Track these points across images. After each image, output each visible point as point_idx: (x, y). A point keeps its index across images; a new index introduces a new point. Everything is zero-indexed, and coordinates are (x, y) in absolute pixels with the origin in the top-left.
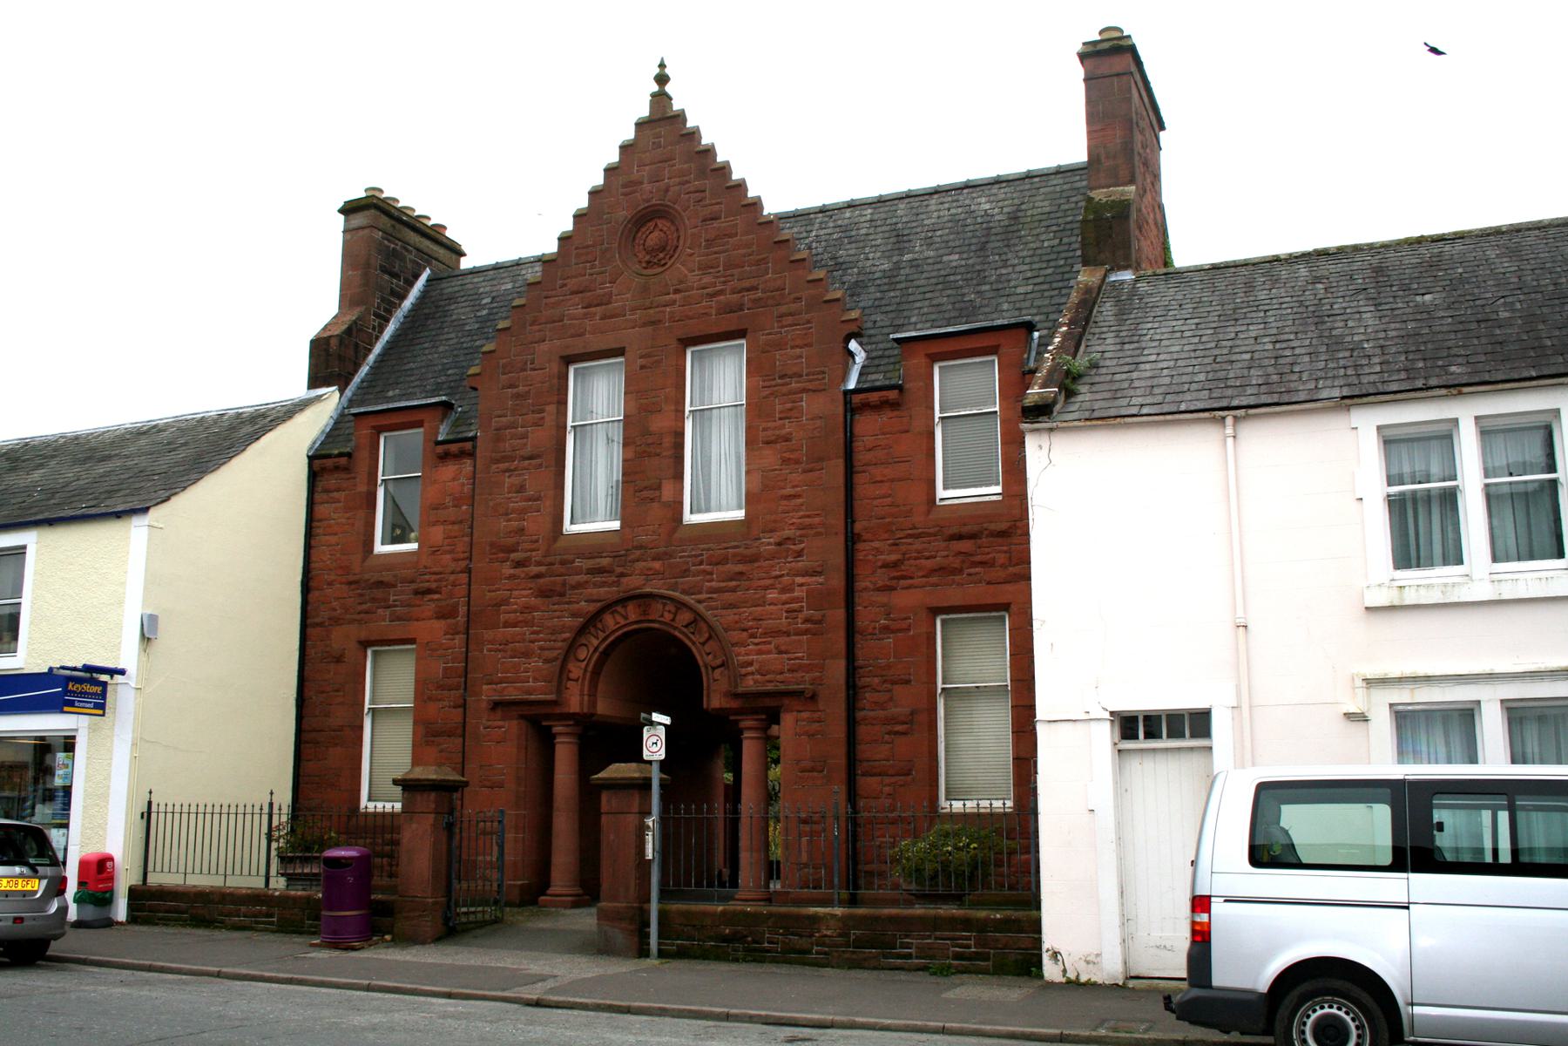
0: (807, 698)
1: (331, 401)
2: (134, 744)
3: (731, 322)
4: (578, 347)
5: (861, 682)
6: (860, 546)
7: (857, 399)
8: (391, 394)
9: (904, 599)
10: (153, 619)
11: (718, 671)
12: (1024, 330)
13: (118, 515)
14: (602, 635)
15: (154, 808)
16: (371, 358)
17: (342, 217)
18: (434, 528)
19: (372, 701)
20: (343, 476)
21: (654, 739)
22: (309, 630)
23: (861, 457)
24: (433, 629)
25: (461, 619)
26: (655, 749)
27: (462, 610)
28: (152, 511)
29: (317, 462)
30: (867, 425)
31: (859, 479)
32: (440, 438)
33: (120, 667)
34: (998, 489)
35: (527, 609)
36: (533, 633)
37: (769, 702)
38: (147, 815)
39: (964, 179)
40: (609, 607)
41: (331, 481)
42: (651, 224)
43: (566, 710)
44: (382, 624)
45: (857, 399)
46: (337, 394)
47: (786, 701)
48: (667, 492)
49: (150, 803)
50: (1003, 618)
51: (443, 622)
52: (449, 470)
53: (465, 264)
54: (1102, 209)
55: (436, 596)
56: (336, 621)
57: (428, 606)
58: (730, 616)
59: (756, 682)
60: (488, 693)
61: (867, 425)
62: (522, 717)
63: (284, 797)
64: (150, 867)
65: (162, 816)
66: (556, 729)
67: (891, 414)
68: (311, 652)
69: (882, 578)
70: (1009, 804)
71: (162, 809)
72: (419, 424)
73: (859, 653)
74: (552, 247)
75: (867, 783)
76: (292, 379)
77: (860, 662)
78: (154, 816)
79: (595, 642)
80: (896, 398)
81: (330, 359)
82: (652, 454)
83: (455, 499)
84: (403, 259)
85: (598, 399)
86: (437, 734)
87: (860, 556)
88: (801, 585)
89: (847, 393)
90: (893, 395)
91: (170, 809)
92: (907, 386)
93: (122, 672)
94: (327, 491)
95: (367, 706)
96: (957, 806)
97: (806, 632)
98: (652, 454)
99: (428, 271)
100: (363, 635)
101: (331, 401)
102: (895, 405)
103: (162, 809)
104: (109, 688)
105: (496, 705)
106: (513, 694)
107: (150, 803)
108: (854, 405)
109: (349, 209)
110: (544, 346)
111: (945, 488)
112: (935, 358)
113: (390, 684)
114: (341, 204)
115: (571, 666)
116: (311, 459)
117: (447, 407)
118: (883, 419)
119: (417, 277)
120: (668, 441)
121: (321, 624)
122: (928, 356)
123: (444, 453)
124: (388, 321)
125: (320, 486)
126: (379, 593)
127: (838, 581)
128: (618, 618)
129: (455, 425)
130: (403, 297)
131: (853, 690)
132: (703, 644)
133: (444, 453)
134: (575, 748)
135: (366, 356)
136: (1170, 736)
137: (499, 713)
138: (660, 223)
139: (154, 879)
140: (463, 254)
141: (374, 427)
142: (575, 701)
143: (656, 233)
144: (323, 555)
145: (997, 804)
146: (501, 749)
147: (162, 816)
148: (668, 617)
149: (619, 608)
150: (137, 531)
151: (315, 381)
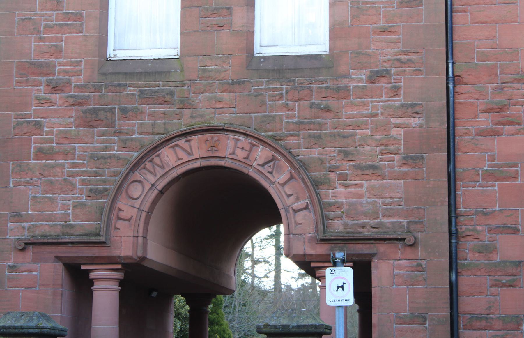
62: (59, 259)
73: (460, 200)
137: (30, 252)
149: (182, 142)
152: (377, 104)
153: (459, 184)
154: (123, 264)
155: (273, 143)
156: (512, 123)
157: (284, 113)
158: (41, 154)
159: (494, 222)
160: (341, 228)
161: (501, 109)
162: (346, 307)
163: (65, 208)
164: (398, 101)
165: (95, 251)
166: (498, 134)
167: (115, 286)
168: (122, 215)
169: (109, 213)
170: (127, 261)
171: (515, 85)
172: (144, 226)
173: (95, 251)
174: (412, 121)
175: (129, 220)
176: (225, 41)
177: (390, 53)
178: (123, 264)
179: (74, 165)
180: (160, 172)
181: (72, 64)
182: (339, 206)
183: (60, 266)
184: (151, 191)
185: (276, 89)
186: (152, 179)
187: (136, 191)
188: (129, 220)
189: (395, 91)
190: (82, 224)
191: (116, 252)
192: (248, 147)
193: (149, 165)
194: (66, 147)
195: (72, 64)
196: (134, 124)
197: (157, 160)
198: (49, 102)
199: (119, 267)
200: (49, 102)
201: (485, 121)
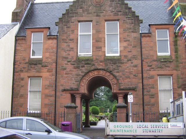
0: (134, 89)
7: (143, 35)
12: (48, 29)
18: (46, 53)
21: (130, 98)
23: (143, 46)
24: (45, 74)
26: (131, 100)
30: (143, 39)
31: (143, 50)
32: (48, 35)
34: (91, 54)
39: (51, 2)
40: (90, 71)
45: (143, 35)
46: (19, 24)
52: (50, 41)
55: (47, 68)
56: (22, 71)
61: (143, 39)
62: (70, 93)
67: (149, 38)
72: (43, 32)
73: (144, 82)
75: (146, 107)
82: (98, 43)
94: (19, 44)
98: (98, 43)
100: (29, 75)
108: (142, 35)
111: (80, 53)
112: (32, 32)
122: (156, 28)
131: (143, 89)
137: (64, 92)
146: (65, 100)
149: (93, 72)
151: (13, 20)
152: (129, 64)
153: (144, 80)
154: (82, 94)
155: (110, 72)
156: (153, 69)
157: (111, 67)
158: (66, 74)
159: (68, 60)
160: (122, 88)
161: (151, 66)
162: (132, 102)
163: (71, 84)
164: (132, 65)
165: (77, 92)
166: (150, 70)
167: (80, 98)
168: (82, 85)
169: (79, 85)
170: (83, 94)
171: (153, 62)
172: (123, 92)
173: (77, 92)
174: (135, 68)
175: (83, 86)
176: (100, 53)
177: (131, 56)
178: (82, 94)
179: (73, 76)
180: (89, 77)
181: (72, 57)
182: (122, 84)
183: (70, 94)
184: (44, 72)
185: (110, 62)
186: (87, 79)
187: (84, 81)
188: (83, 86)
189: (132, 63)
190: (74, 87)
191: (80, 92)
192: (105, 73)
193: (87, 76)
194: (71, 72)
195: (72, 57)
196: (83, 69)
197: (88, 75)
198: (67, 64)
199: (81, 95)
200: (67, 64)
201: (148, 68)
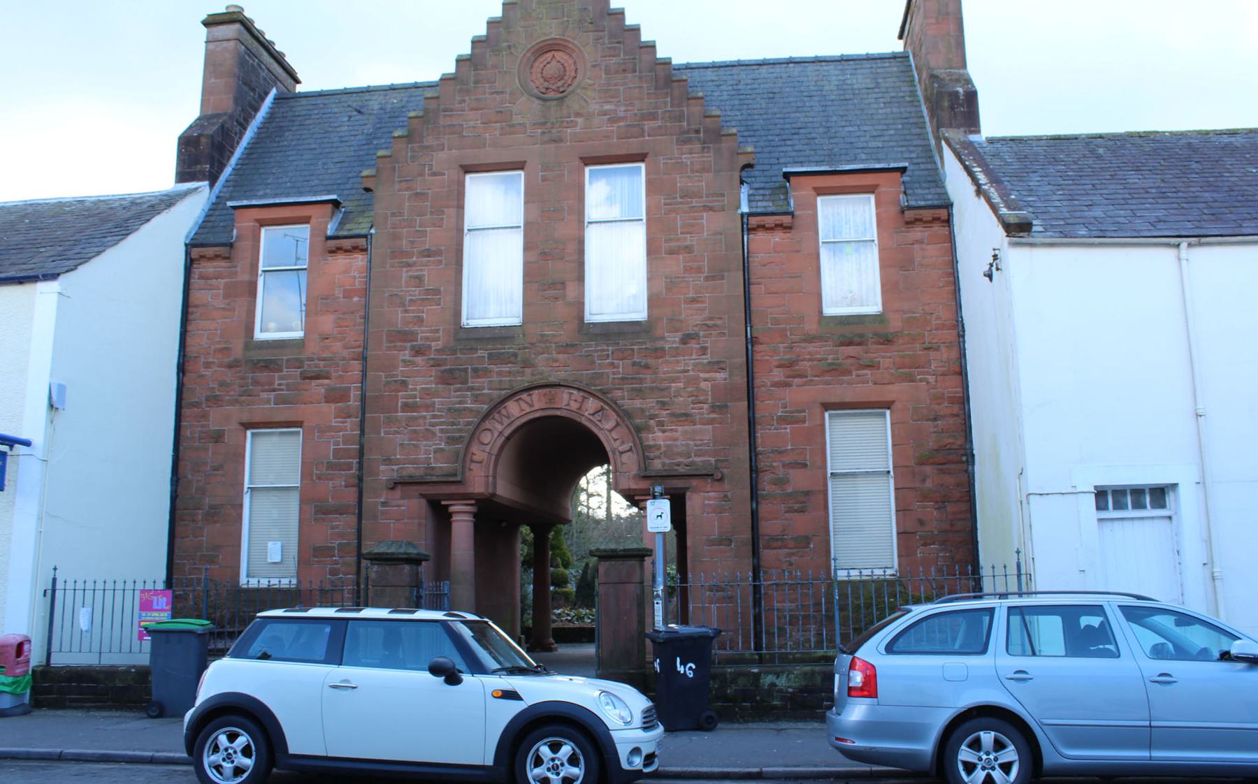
1: (200, 198)
2: (40, 519)
3: (633, 146)
4: (472, 157)
5: (761, 465)
6: (758, 348)
8: (261, 193)
9: (799, 394)
10: (62, 388)
11: (625, 456)
13: (20, 281)
14: (506, 422)
15: (59, 585)
16: (233, 161)
17: (204, 30)
19: (251, 482)
20: (223, 264)
22: (186, 412)
24: (322, 412)
25: (354, 402)
27: (354, 394)
28: (62, 277)
29: (195, 252)
32: (329, 233)
33: (24, 436)
35: (427, 393)
36: (434, 417)
37: (679, 484)
38: (51, 593)
39: (787, 56)
41: (208, 268)
42: (549, 55)
43: (471, 490)
44: (265, 406)
45: (754, 221)
46: (207, 189)
47: (694, 482)
48: (571, 292)
49: (54, 580)
50: (884, 415)
51: (333, 406)
53: (299, 89)
54: (929, 88)
55: (326, 381)
56: (214, 400)
57: (317, 388)
58: (638, 403)
59: (664, 465)
60: (385, 473)
62: (422, 496)
63: (160, 574)
64: (55, 647)
65: (70, 594)
66: (452, 509)
68: (186, 433)
69: (778, 375)
70: (294, 581)
71: (70, 585)
72: (305, 220)
74: (451, 68)
75: (767, 555)
76: (156, 171)
77: (760, 449)
78: (59, 594)
79: (500, 428)
80: (784, 219)
81: (200, 153)
82: (554, 257)
83: (345, 291)
84: (258, 76)
85: (494, 209)
86: (327, 512)
87: (758, 357)
88: (706, 380)
89: (742, 215)
90: (786, 220)
91: (80, 585)
92: (797, 213)
93: (27, 443)
95: (246, 485)
96: (253, 583)
97: (711, 422)
98: (554, 257)
99: (274, 92)
100: (246, 418)
101: (200, 198)
102: (787, 228)
103: (70, 585)
104: (9, 459)
105: (395, 485)
106: (410, 470)
107: (54, 580)
109: (211, 22)
110: (442, 155)
113: (272, 464)
114: (204, 17)
115: (475, 448)
116: (189, 247)
117: (336, 204)
118: (777, 237)
119: (267, 94)
120: (571, 248)
121: (197, 405)
122: (815, 189)
123: (334, 246)
124: (245, 129)
125: (196, 271)
126: (263, 376)
127: (741, 380)
128: (524, 406)
129: (342, 224)
130: (256, 110)
131: (754, 470)
132: (610, 431)
133: (334, 246)
134: (471, 525)
135: (229, 158)
136: (1115, 508)
137: (398, 492)
138: (559, 55)
139: (58, 660)
140: (298, 81)
141: (257, 220)
142: (478, 483)
143: (554, 63)
144: (198, 342)
145: (274, 581)
147: (70, 594)
148: (574, 406)
150: (46, 292)
